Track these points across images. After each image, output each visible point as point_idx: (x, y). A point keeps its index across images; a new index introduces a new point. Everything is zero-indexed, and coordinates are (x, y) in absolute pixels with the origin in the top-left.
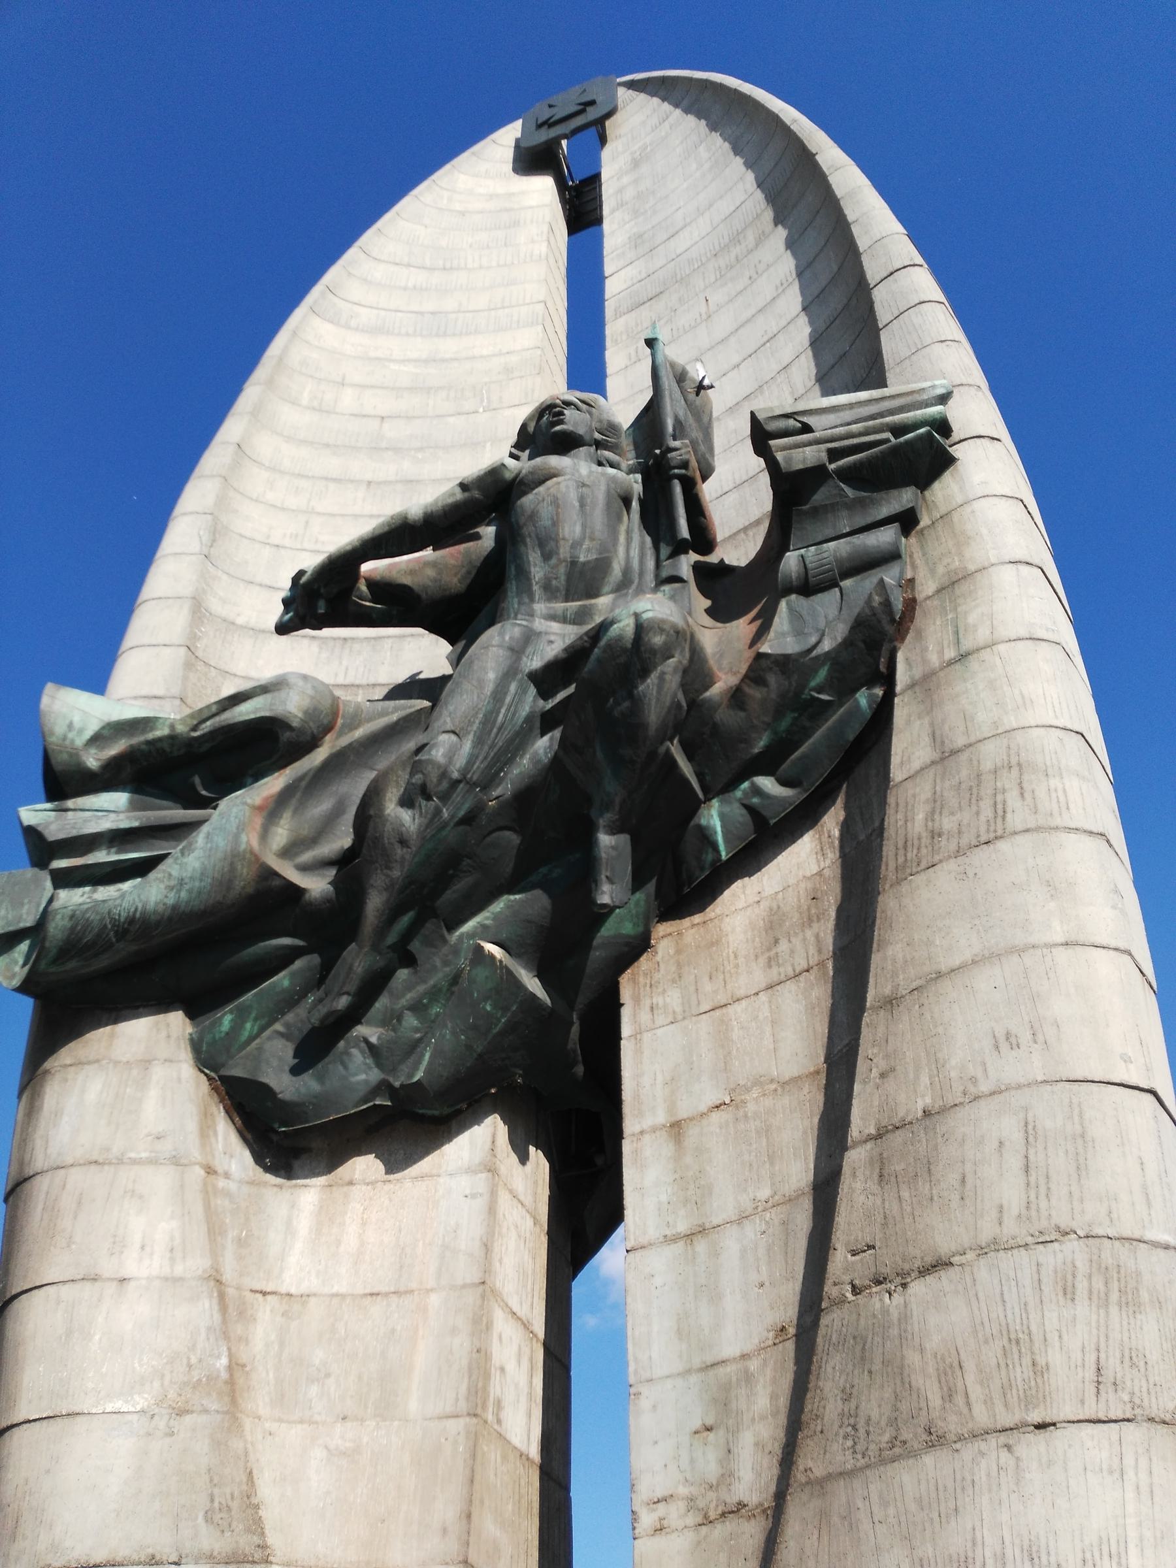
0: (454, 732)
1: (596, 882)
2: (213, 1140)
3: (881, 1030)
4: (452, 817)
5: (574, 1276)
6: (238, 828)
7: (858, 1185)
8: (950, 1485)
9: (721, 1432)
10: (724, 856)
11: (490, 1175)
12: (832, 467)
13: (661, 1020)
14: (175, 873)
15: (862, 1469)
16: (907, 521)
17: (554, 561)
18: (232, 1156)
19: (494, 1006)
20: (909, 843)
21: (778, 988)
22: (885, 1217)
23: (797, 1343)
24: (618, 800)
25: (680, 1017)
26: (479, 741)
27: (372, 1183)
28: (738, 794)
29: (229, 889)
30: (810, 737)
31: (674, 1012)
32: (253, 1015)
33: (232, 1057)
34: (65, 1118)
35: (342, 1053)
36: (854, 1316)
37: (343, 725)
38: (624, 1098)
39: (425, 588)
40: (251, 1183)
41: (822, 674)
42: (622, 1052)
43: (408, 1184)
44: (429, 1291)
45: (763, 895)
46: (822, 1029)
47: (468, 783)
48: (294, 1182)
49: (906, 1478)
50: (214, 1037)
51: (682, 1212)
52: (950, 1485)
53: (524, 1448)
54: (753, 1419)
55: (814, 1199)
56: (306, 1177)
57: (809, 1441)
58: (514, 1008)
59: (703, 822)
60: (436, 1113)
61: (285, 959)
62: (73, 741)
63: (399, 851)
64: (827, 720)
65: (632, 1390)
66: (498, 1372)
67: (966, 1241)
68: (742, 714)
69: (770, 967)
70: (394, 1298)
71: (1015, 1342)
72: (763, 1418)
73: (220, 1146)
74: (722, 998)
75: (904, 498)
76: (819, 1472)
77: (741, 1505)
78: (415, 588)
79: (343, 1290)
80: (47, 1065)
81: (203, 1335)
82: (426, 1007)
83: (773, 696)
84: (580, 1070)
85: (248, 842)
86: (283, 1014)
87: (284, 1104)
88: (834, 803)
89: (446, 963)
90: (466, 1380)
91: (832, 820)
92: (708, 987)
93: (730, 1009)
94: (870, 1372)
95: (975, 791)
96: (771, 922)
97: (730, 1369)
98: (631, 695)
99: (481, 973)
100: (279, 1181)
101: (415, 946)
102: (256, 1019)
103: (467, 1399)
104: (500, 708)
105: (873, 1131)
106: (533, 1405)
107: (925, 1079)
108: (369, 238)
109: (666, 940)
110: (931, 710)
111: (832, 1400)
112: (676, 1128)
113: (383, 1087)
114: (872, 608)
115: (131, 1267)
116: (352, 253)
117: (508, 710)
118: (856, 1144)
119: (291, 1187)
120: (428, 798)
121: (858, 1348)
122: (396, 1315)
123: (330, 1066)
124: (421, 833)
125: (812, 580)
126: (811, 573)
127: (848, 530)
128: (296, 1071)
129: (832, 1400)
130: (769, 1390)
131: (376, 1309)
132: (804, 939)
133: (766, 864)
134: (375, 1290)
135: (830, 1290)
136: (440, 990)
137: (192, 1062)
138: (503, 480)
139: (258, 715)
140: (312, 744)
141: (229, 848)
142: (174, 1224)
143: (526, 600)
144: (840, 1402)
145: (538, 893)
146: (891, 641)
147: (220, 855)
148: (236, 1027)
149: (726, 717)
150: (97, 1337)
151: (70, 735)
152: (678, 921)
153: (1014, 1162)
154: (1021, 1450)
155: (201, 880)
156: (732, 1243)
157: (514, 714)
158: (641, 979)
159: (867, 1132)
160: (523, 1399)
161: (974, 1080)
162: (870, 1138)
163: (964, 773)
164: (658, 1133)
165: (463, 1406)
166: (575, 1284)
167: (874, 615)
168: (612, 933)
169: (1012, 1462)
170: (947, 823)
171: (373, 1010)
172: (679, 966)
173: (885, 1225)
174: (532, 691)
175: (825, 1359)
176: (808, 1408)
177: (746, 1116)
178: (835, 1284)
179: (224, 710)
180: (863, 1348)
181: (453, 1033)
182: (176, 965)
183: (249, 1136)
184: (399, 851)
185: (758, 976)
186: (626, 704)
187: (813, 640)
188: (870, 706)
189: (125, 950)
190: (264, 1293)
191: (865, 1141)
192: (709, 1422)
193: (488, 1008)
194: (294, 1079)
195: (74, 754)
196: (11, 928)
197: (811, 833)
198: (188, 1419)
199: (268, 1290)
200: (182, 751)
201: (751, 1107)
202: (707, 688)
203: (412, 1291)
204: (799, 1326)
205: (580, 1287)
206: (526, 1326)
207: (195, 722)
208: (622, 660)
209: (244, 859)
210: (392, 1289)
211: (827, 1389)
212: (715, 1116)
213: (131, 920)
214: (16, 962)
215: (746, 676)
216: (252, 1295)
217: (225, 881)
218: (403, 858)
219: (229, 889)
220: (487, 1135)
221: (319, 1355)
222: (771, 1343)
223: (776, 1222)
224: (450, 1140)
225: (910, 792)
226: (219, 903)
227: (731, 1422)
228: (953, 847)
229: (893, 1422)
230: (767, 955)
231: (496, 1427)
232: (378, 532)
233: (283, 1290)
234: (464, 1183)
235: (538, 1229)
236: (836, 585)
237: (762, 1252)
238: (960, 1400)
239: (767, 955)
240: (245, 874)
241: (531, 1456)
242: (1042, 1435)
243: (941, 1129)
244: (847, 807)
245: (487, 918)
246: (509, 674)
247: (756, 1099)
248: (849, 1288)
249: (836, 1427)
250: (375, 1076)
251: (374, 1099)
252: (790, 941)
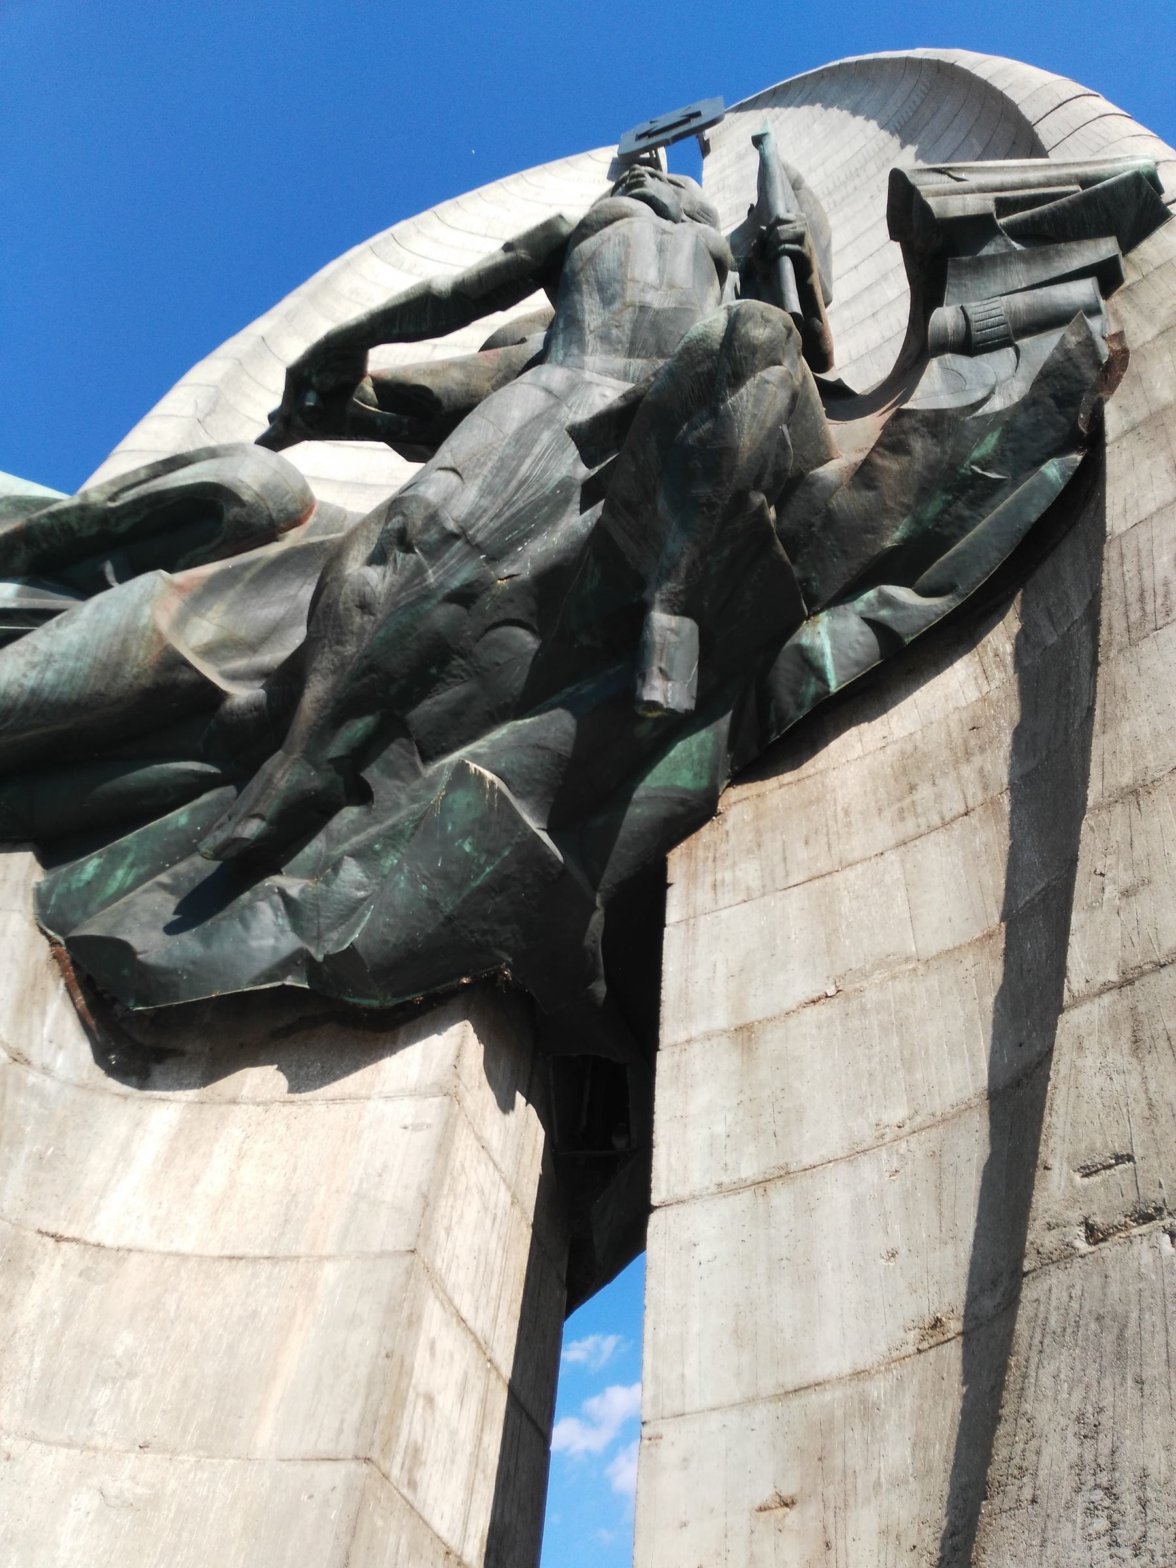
0: (454, 470)
1: (644, 677)
2: (36, 1021)
4: (441, 585)
5: (570, 1309)
6: (141, 599)
7: (1090, 1061)
10: (834, 687)
11: (447, 1100)
12: (1001, 221)
13: (726, 898)
16: (1108, 277)
17: (617, 305)
18: (60, 1048)
19: (476, 846)
20: (1148, 595)
21: (917, 842)
22: (1151, 1106)
23: (966, 1347)
24: (684, 562)
25: (757, 894)
26: (488, 491)
27: (266, 1104)
29: (115, 676)
30: (968, 531)
31: (748, 888)
32: (130, 859)
35: (243, 907)
36: (1096, 1280)
37: (315, 525)
38: (663, 997)
39: (448, 392)
40: (82, 1087)
41: (991, 442)
42: (664, 956)
43: (320, 1108)
44: (322, 1259)
45: (889, 740)
47: (468, 542)
48: (148, 1093)
50: (69, 889)
51: (751, 1149)
53: (454, 1543)
54: (877, 1485)
55: (992, 1114)
56: (168, 1088)
57: (1004, 1520)
58: (506, 853)
59: (805, 640)
60: (375, 1003)
63: (358, 619)
64: (993, 507)
65: (647, 1431)
66: (421, 1403)
68: (871, 494)
69: (902, 819)
70: (266, 1266)
72: (897, 1483)
73: (46, 1030)
74: (823, 865)
75: (1107, 247)
78: (435, 390)
79: (186, 1248)
83: (918, 467)
84: (600, 989)
85: (152, 616)
86: (173, 863)
87: (145, 970)
88: (1002, 616)
89: (413, 800)
90: (360, 1402)
91: (1001, 638)
92: (801, 854)
93: (838, 878)
94: (1140, 1381)
96: (904, 768)
97: (829, 1396)
98: (715, 413)
99: (462, 799)
100: (126, 1089)
101: (372, 774)
102: (132, 865)
103: (358, 1432)
104: (525, 457)
105: (1114, 977)
106: (480, 1476)
108: (446, 208)
109: (740, 806)
111: (1054, 1438)
112: (745, 1034)
114: (1067, 352)
116: (426, 215)
117: (536, 462)
119: (141, 1099)
120: (408, 548)
121: (1108, 1340)
122: (264, 1291)
123: (224, 923)
124: (392, 595)
125: (977, 335)
126: (974, 326)
127: (1024, 285)
128: (172, 929)
129: (1054, 1438)
130: (910, 1431)
131: (233, 1280)
133: (895, 703)
134: (238, 1252)
135: (1038, 1236)
136: (401, 833)
137: (31, 917)
138: (559, 235)
139: (198, 480)
140: (269, 532)
141: (123, 622)
143: (575, 351)
144: (1073, 1442)
145: (560, 711)
146: (1095, 390)
147: (109, 629)
148: (103, 875)
149: (845, 501)
152: (759, 783)
155: (78, 659)
156: (836, 1194)
157: (544, 471)
158: (701, 853)
159: (1101, 979)
160: (463, 1460)
162: (1107, 988)
164: (715, 1041)
165: (349, 1443)
166: (566, 1323)
167: (1070, 359)
168: (661, 783)
171: (300, 856)
172: (758, 832)
174: (573, 451)
175: (1034, 1360)
176: (1001, 1452)
177: (863, 1009)
178: (1050, 1227)
179: (156, 476)
180: (1121, 1336)
181: (412, 881)
183: (92, 1023)
184: (358, 619)
185: (884, 832)
186: (708, 425)
187: (979, 395)
188: (1063, 475)
190: (58, 1238)
191: (1100, 994)
192: (788, 1491)
193: (467, 848)
194: (168, 937)
197: (966, 658)
199: (68, 1234)
200: (95, 529)
201: (871, 997)
202: (823, 461)
203: (297, 1257)
204: (971, 1315)
205: (581, 1347)
206: (482, 1347)
207: (115, 489)
208: (706, 366)
209: (143, 636)
210: (266, 1253)
211: (1042, 1418)
212: (811, 1013)
215: (879, 443)
216: (39, 1237)
217: (112, 667)
218: (362, 627)
219: (115, 676)
220: (448, 1054)
221: (124, 1342)
222: (911, 1349)
223: (919, 1154)
224: (393, 1051)
226: (100, 694)
227: (830, 1491)
230: (898, 805)
231: (405, 1491)
232: (390, 305)
233: (92, 1238)
234: (406, 1110)
235: (517, 1212)
236: (1008, 343)
239: (898, 805)
240: (142, 657)
241: (466, 1559)
244: (1023, 616)
245: (481, 747)
246: (541, 419)
248: (1081, 1231)
249: (1066, 1492)
250: (290, 943)
251: (284, 977)
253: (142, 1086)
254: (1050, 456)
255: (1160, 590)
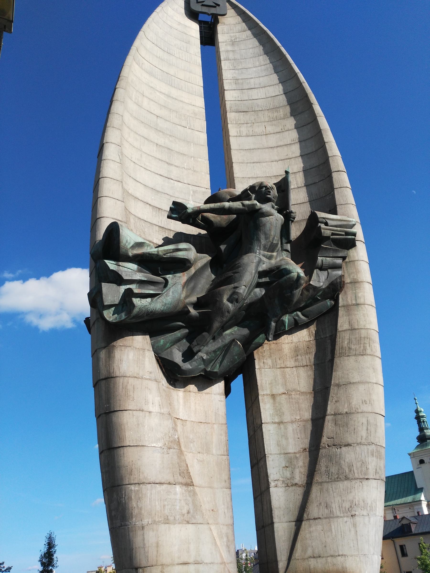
3: (336, 391)
8: (350, 487)
9: (290, 468)
14: (164, 301)
15: (330, 482)
16: (344, 258)
17: (268, 241)
28: (293, 315)
33: (163, 352)
34: (124, 362)
46: (312, 382)
49: (341, 485)
51: (276, 417)
52: (350, 487)
59: (284, 319)
61: (179, 328)
62: (127, 246)
67: (355, 442)
71: (363, 463)
72: (301, 467)
74: (283, 366)
76: (320, 480)
77: (296, 484)
80: (114, 343)
81: (171, 430)
82: (216, 352)
88: (313, 324)
92: (279, 362)
98: (291, 292)
100: (173, 388)
102: (170, 343)
107: (346, 406)
110: (349, 315)
113: (205, 370)
114: (337, 282)
115: (151, 409)
118: (329, 415)
121: (330, 458)
127: (331, 256)
131: (202, 426)
132: (306, 358)
138: (255, 208)
142: (159, 398)
147: (176, 299)
150: (146, 427)
151: (127, 244)
153: (365, 428)
154: (363, 483)
156: (290, 428)
161: (357, 408)
162: (332, 415)
163: (357, 336)
169: (362, 485)
170: (353, 347)
173: (336, 434)
176: (317, 468)
182: (153, 325)
184: (227, 314)
186: (290, 294)
189: (146, 318)
192: (287, 465)
195: (127, 250)
196: (112, 303)
198: (171, 450)
208: (292, 283)
211: (322, 465)
212: (283, 396)
213: (151, 312)
214: (111, 313)
217: (175, 307)
220: (106, 303)
221: (191, 436)
225: (343, 335)
228: (354, 353)
229: (337, 474)
237: (298, 431)
238: (352, 472)
242: (367, 481)
243: (350, 417)
247: (294, 394)
249: (324, 473)
253: (175, 388)
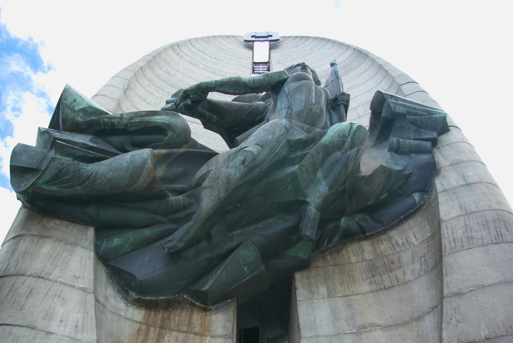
20: (456, 240)
95: (486, 226)
115: (54, 327)
142: (80, 316)
200: (122, 127)
236: (409, 154)
252: (381, 276)
254: (416, 192)
255: (460, 240)
